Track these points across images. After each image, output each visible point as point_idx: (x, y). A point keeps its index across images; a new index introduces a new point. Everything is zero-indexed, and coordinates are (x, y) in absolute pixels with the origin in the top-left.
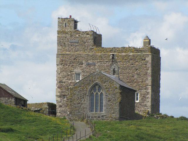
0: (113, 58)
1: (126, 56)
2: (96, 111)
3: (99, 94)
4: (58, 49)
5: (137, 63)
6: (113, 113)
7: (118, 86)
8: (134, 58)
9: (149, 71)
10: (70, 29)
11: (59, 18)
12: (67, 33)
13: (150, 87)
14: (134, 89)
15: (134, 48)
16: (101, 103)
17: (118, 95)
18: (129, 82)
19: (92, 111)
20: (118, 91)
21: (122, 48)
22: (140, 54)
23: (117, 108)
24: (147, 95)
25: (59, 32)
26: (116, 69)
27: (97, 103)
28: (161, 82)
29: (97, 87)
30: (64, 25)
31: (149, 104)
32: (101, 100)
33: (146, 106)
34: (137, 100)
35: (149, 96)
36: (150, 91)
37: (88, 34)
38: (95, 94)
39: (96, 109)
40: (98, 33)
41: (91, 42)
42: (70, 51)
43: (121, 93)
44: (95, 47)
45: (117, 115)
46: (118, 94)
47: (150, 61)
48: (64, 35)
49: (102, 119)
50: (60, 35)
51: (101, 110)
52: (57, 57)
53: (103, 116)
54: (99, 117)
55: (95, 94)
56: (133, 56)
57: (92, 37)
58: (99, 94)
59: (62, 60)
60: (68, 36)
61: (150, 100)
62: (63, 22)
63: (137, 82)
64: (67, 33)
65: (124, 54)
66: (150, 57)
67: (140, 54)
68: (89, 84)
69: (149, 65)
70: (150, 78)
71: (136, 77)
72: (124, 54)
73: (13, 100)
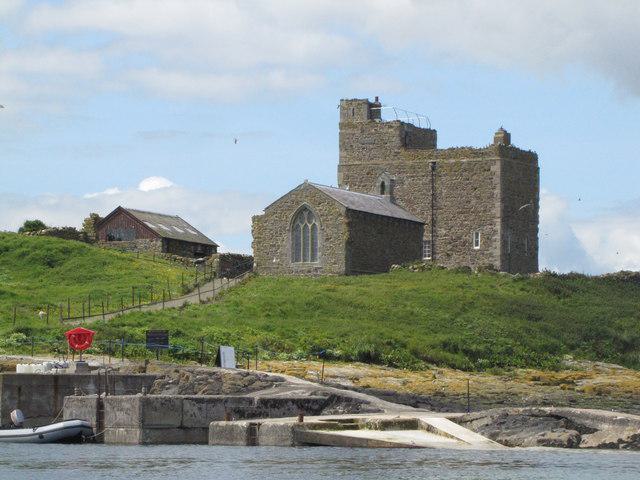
0: (433, 169)
1: (456, 164)
2: (305, 260)
3: (310, 226)
4: (341, 157)
5: (475, 177)
6: (335, 264)
7: (343, 210)
8: (470, 168)
9: (497, 191)
10: (362, 117)
11: (342, 100)
12: (354, 127)
13: (499, 220)
14: (418, 219)
15: (470, 149)
16: (314, 244)
17: (344, 228)
18: (461, 213)
19: (297, 260)
20: (343, 219)
21: (449, 149)
22: (480, 159)
23: (341, 253)
24: (494, 235)
25: (342, 126)
26: (386, 184)
27: (305, 244)
28: (539, 213)
29: (306, 214)
30: (350, 112)
31: (497, 252)
32: (314, 238)
33: (491, 255)
34: (477, 245)
35: (498, 237)
36: (498, 227)
37: (391, 127)
38: (302, 226)
39: (304, 256)
40: (417, 125)
41: (396, 141)
42: (360, 160)
43: (348, 224)
44: (402, 151)
45: (341, 267)
46: (344, 226)
47: (498, 173)
48: (350, 131)
49: (315, 276)
50: (343, 131)
51: (313, 258)
52: (339, 171)
53: (316, 269)
54: (309, 272)
55: (302, 226)
56: (469, 163)
57: (398, 133)
58: (310, 226)
59: (348, 177)
60: (357, 132)
61: (498, 244)
62: (349, 107)
63: (476, 212)
64: (354, 127)
65: (452, 161)
66: (498, 164)
67: (480, 159)
68: (289, 209)
69: (497, 180)
70: (498, 204)
71: (473, 202)
72: (452, 161)
73: (159, 243)
